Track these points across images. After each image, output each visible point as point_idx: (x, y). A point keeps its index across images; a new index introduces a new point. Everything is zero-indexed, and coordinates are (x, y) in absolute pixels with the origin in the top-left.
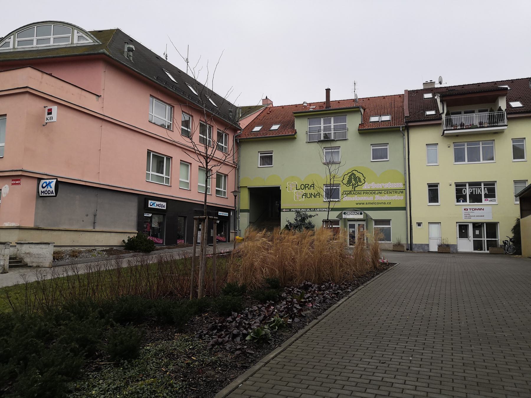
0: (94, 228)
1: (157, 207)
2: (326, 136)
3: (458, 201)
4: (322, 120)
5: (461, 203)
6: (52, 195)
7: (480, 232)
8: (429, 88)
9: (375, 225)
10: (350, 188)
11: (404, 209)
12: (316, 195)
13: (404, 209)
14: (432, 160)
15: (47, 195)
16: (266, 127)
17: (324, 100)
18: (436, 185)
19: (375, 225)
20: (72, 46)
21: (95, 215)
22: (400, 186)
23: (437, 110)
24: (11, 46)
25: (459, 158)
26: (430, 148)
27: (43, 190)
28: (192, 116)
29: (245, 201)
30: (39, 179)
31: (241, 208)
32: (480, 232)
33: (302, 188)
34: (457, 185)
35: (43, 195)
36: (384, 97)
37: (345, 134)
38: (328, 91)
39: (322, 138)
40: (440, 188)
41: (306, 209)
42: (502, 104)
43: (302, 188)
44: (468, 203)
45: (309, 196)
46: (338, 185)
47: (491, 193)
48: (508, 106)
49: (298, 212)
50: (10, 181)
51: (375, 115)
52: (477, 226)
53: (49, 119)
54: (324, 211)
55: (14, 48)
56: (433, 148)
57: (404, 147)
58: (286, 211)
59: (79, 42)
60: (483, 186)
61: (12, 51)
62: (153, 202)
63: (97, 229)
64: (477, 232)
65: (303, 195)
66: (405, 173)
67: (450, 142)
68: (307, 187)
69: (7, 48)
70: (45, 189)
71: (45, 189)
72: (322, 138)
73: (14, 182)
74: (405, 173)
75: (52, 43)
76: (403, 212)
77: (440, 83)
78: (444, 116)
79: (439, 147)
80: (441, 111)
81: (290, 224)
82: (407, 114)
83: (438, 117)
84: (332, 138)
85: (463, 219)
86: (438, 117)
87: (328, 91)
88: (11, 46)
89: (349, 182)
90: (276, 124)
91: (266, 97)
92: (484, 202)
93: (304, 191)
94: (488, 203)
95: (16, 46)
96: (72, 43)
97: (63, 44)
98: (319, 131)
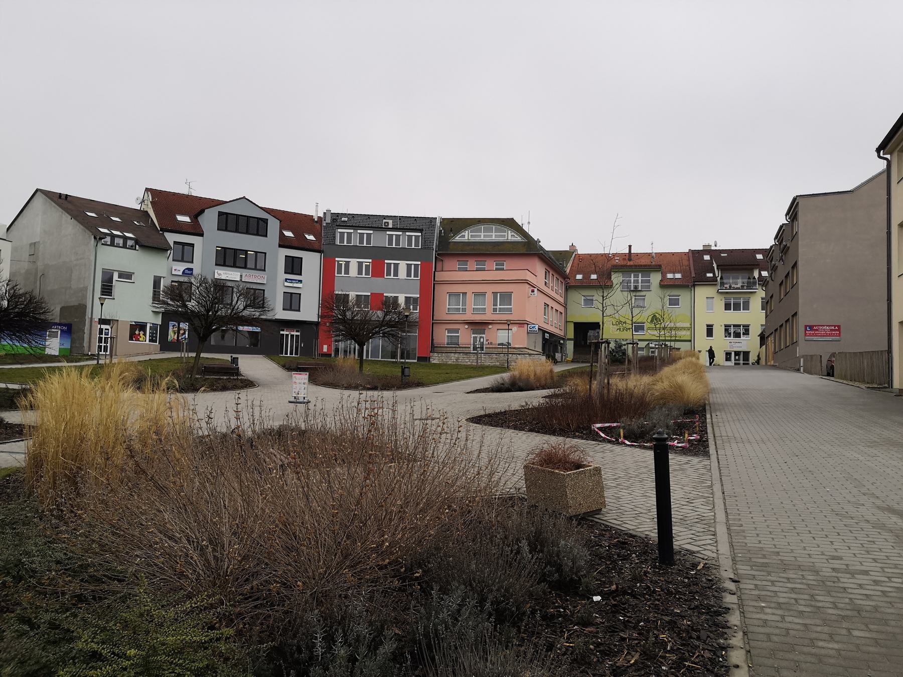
2: (636, 287)
3: (726, 337)
5: (728, 338)
7: (739, 358)
8: (707, 251)
10: (653, 325)
11: (690, 341)
13: (690, 341)
14: (710, 307)
16: (587, 276)
17: (627, 252)
18: (712, 326)
22: (688, 325)
23: (714, 274)
24: (466, 238)
25: (727, 307)
26: (709, 300)
28: (549, 272)
30: (528, 324)
32: (739, 358)
34: (726, 326)
36: (673, 254)
37: (649, 287)
38: (630, 246)
39: (632, 289)
40: (714, 328)
42: (756, 274)
44: (732, 338)
46: (644, 323)
47: (747, 332)
48: (760, 274)
50: (517, 325)
51: (670, 272)
52: (737, 353)
55: (468, 239)
56: (711, 300)
57: (691, 298)
60: (742, 327)
64: (737, 357)
66: (691, 317)
67: (722, 297)
74: (691, 317)
75: (494, 238)
76: (689, 343)
77: (716, 246)
78: (719, 279)
79: (714, 299)
80: (717, 276)
82: (693, 275)
83: (714, 279)
84: (640, 289)
85: (729, 349)
86: (714, 279)
87: (630, 246)
88: (466, 238)
89: (652, 321)
92: (742, 337)
94: (744, 338)
96: (507, 239)
97: (501, 239)
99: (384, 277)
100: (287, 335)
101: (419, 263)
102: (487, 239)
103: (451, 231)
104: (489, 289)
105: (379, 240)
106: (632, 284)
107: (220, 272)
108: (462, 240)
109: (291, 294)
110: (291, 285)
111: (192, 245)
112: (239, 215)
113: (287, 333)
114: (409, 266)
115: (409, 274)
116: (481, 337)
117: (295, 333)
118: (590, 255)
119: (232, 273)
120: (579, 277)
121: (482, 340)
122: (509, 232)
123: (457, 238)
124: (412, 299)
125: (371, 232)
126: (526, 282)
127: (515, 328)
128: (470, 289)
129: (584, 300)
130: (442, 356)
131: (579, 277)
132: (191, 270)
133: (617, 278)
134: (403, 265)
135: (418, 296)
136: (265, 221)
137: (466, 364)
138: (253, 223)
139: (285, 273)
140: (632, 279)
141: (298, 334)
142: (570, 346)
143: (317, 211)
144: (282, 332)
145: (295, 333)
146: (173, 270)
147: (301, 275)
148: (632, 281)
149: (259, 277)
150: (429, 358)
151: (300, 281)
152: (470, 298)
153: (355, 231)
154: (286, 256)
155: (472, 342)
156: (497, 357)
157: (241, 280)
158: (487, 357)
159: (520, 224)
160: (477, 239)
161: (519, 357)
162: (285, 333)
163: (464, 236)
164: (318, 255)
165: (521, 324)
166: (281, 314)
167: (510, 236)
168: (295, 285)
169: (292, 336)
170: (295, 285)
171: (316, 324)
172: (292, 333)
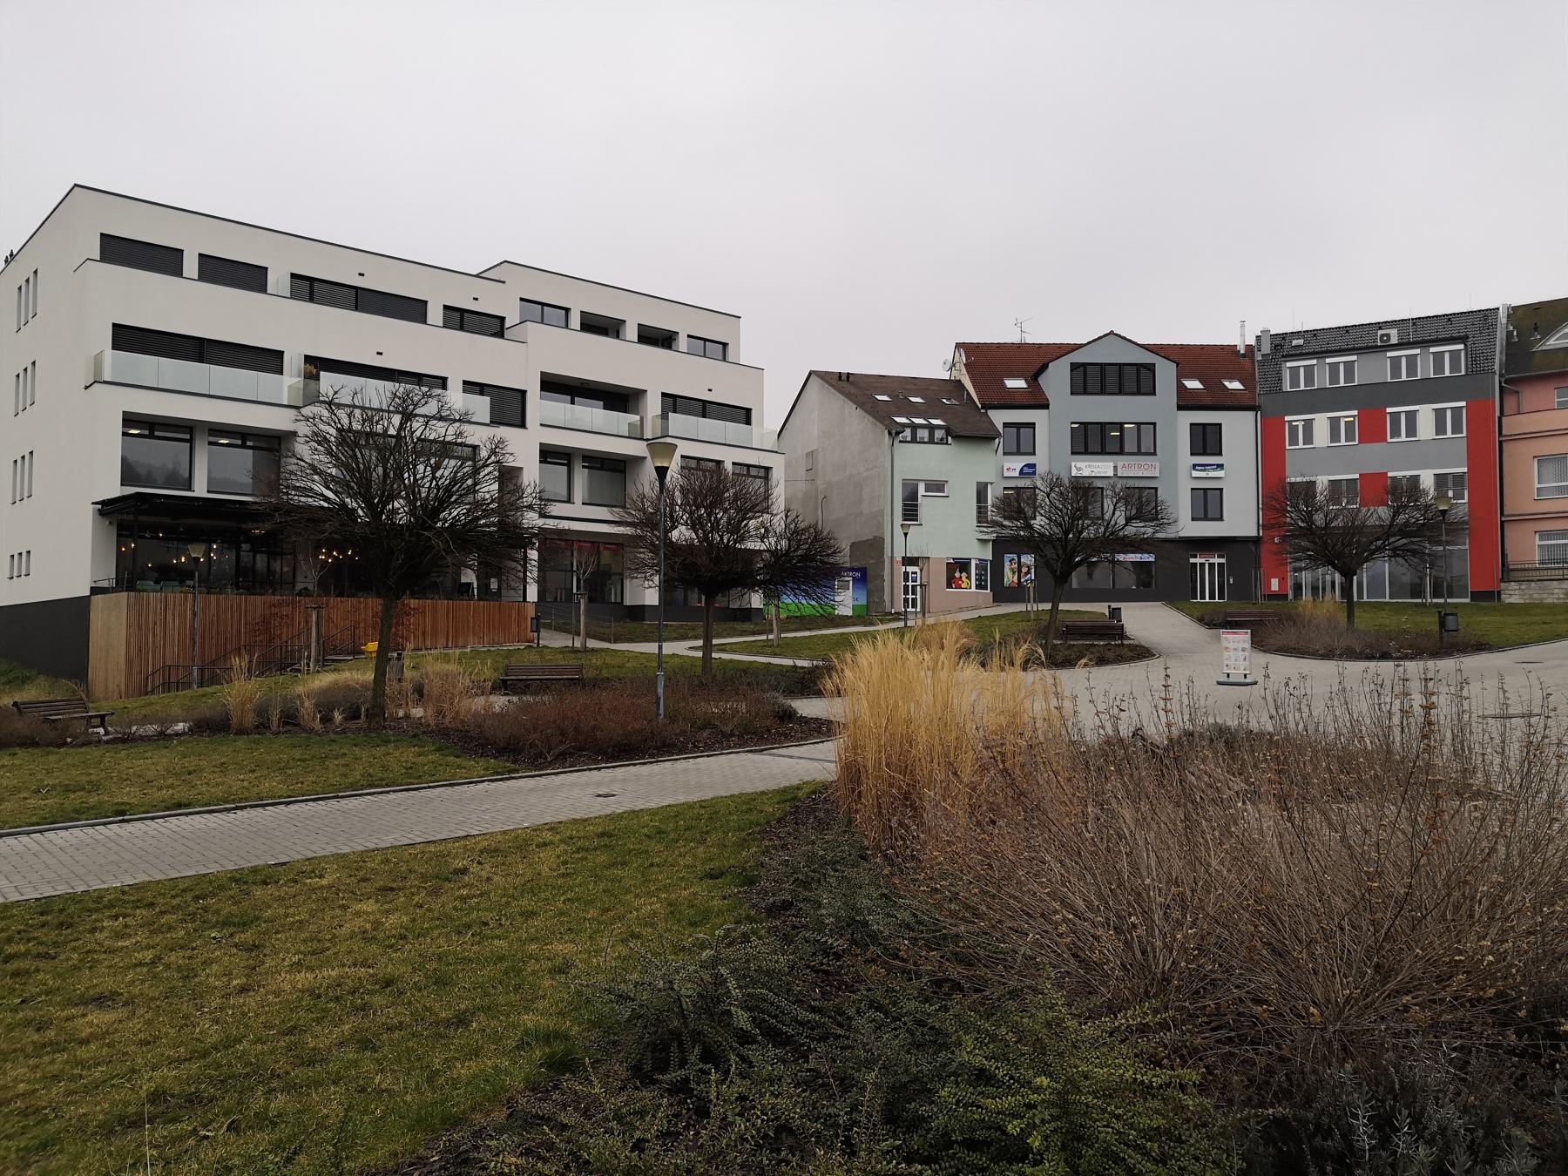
99: (1385, 440)
100: (1202, 565)
101: (1463, 404)
105: (1372, 370)
107: (1079, 465)
109: (1205, 490)
110: (1203, 474)
111: (1032, 425)
112: (1105, 364)
113: (1203, 561)
117: (1216, 560)
119: (1100, 464)
123: (1551, 342)
124: (1450, 477)
132: (1033, 466)
134: (1425, 414)
135: (1465, 470)
136: (1150, 368)
141: (1223, 561)
144: (1192, 560)
145: (1216, 560)
147: (1220, 454)
151: (1220, 466)
153: (1320, 360)
162: (1198, 560)
166: (1189, 527)
168: (1212, 474)
169: (1212, 565)
170: (1212, 474)
171: (1256, 541)
172: (1212, 561)
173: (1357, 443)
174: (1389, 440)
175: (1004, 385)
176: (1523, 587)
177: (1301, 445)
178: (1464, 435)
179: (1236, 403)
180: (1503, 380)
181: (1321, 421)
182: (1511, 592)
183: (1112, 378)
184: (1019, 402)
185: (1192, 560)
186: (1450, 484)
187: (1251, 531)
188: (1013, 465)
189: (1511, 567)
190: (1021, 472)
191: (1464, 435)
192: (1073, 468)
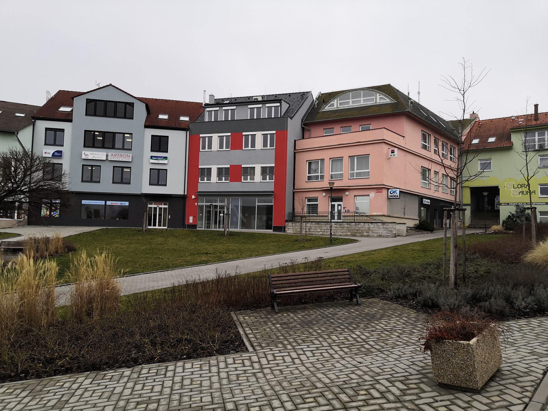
0: (404, 216)
1: (427, 203)
4: (537, 134)
6: (397, 197)
9: (540, 215)
12: (532, 192)
15: (394, 197)
16: (484, 140)
19: (540, 215)
20: (376, 104)
21: (404, 209)
24: (335, 106)
27: (391, 195)
29: (467, 198)
30: (388, 189)
31: (464, 203)
33: (519, 187)
35: (391, 197)
38: (536, 106)
39: (537, 148)
41: (523, 203)
43: (519, 187)
45: (525, 193)
49: (517, 206)
53: (393, 155)
54: (540, 204)
55: (337, 107)
58: (504, 205)
59: (380, 101)
61: (336, 109)
62: (425, 200)
63: (405, 217)
65: (520, 193)
68: (524, 186)
69: (333, 107)
70: (392, 195)
71: (392, 195)
72: (537, 148)
73: (378, 191)
75: (362, 103)
81: (513, 215)
87: (536, 106)
88: (335, 106)
90: (492, 136)
91: (473, 112)
93: (521, 190)
95: (339, 106)
96: (376, 102)
97: (369, 103)
98: (534, 142)
99: (242, 149)
100: (155, 209)
101: (274, 132)
102: (356, 105)
103: (324, 102)
104: (345, 153)
105: (243, 114)
106: (537, 143)
107: (86, 153)
108: (331, 108)
109: (159, 170)
110: (156, 161)
111: (63, 130)
112: (117, 102)
113: (156, 206)
114: (265, 136)
115: (265, 145)
116: (339, 205)
117: (163, 206)
118: (491, 120)
119: (99, 153)
120: (475, 141)
121: (339, 207)
122: (378, 95)
123: (326, 108)
124: (268, 169)
125: (234, 107)
126: (384, 142)
127: (372, 194)
128: (327, 155)
129: (480, 163)
130: (295, 226)
131: (475, 141)
132: (60, 152)
133: (517, 140)
134: (259, 135)
135: (273, 165)
136: (132, 105)
137: (318, 233)
138: (121, 108)
139: (152, 151)
140: (537, 138)
141: (166, 206)
142: (468, 213)
143: (204, 98)
144: (150, 206)
145: (163, 206)
146: (44, 153)
147: (167, 152)
148: (537, 140)
149: (124, 156)
150: (285, 227)
151: (166, 158)
152: (328, 164)
153: (221, 108)
154: (152, 136)
155: (330, 210)
156: (348, 226)
157: (107, 159)
158: (338, 226)
159: (407, 94)
160: (346, 106)
161: (372, 226)
162: (153, 206)
163: (333, 105)
164: (183, 133)
165: (379, 188)
166: (148, 189)
167: (380, 99)
168: (161, 162)
169: (160, 209)
170: (161, 162)
171: (182, 198)
172: (160, 206)
173: (230, 149)
174: (244, 149)
175: (190, 119)
176: (294, 225)
177: (207, 150)
178: (274, 148)
179: (177, 126)
180: (302, 123)
181: (215, 137)
182: (289, 227)
183: (110, 108)
184: (163, 125)
185: (150, 206)
186: (268, 171)
187: (181, 192)
188: (48, 151)
189: (296, 214)
190: (53, 155)
191: (274, 148)
192: (83, 154)
